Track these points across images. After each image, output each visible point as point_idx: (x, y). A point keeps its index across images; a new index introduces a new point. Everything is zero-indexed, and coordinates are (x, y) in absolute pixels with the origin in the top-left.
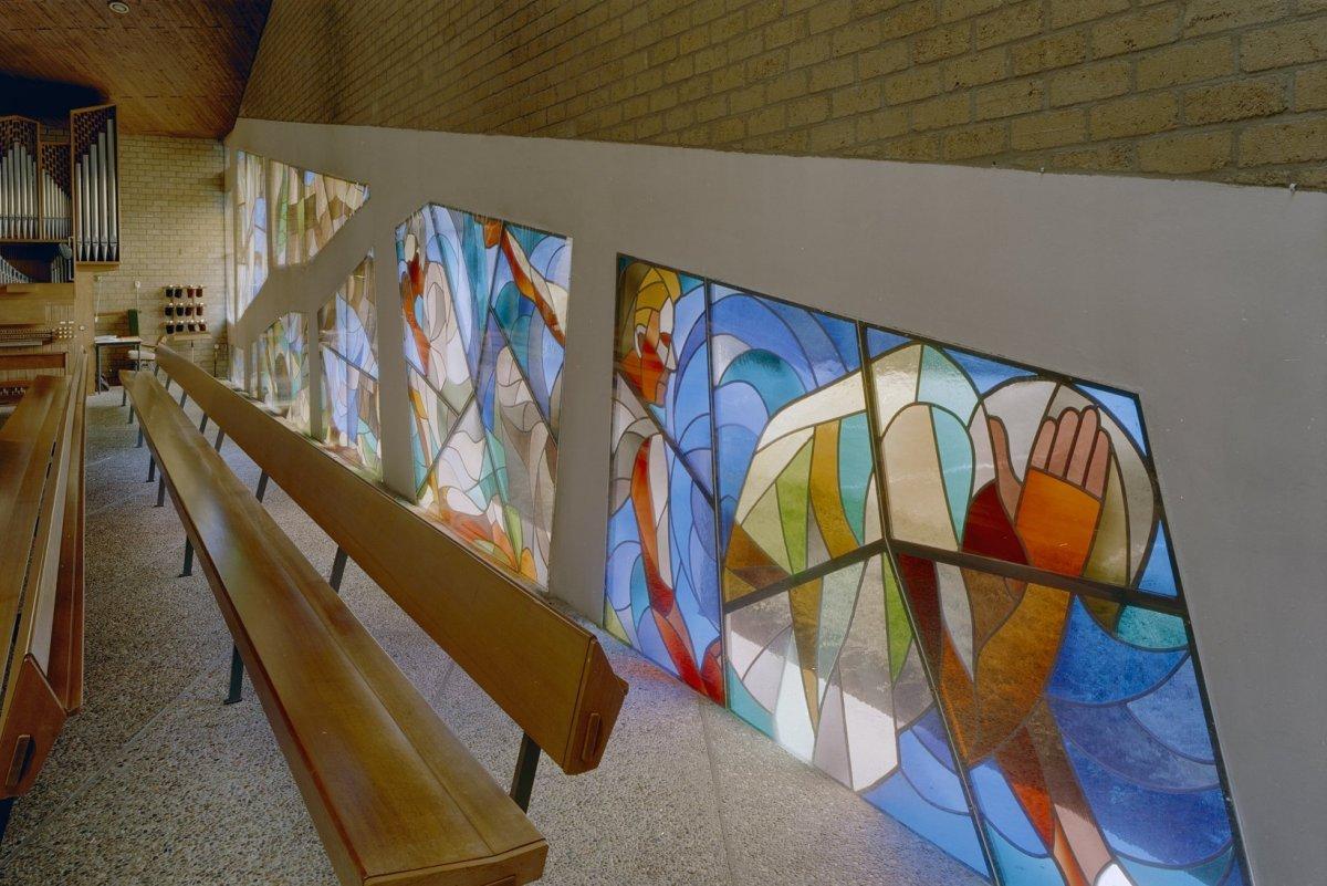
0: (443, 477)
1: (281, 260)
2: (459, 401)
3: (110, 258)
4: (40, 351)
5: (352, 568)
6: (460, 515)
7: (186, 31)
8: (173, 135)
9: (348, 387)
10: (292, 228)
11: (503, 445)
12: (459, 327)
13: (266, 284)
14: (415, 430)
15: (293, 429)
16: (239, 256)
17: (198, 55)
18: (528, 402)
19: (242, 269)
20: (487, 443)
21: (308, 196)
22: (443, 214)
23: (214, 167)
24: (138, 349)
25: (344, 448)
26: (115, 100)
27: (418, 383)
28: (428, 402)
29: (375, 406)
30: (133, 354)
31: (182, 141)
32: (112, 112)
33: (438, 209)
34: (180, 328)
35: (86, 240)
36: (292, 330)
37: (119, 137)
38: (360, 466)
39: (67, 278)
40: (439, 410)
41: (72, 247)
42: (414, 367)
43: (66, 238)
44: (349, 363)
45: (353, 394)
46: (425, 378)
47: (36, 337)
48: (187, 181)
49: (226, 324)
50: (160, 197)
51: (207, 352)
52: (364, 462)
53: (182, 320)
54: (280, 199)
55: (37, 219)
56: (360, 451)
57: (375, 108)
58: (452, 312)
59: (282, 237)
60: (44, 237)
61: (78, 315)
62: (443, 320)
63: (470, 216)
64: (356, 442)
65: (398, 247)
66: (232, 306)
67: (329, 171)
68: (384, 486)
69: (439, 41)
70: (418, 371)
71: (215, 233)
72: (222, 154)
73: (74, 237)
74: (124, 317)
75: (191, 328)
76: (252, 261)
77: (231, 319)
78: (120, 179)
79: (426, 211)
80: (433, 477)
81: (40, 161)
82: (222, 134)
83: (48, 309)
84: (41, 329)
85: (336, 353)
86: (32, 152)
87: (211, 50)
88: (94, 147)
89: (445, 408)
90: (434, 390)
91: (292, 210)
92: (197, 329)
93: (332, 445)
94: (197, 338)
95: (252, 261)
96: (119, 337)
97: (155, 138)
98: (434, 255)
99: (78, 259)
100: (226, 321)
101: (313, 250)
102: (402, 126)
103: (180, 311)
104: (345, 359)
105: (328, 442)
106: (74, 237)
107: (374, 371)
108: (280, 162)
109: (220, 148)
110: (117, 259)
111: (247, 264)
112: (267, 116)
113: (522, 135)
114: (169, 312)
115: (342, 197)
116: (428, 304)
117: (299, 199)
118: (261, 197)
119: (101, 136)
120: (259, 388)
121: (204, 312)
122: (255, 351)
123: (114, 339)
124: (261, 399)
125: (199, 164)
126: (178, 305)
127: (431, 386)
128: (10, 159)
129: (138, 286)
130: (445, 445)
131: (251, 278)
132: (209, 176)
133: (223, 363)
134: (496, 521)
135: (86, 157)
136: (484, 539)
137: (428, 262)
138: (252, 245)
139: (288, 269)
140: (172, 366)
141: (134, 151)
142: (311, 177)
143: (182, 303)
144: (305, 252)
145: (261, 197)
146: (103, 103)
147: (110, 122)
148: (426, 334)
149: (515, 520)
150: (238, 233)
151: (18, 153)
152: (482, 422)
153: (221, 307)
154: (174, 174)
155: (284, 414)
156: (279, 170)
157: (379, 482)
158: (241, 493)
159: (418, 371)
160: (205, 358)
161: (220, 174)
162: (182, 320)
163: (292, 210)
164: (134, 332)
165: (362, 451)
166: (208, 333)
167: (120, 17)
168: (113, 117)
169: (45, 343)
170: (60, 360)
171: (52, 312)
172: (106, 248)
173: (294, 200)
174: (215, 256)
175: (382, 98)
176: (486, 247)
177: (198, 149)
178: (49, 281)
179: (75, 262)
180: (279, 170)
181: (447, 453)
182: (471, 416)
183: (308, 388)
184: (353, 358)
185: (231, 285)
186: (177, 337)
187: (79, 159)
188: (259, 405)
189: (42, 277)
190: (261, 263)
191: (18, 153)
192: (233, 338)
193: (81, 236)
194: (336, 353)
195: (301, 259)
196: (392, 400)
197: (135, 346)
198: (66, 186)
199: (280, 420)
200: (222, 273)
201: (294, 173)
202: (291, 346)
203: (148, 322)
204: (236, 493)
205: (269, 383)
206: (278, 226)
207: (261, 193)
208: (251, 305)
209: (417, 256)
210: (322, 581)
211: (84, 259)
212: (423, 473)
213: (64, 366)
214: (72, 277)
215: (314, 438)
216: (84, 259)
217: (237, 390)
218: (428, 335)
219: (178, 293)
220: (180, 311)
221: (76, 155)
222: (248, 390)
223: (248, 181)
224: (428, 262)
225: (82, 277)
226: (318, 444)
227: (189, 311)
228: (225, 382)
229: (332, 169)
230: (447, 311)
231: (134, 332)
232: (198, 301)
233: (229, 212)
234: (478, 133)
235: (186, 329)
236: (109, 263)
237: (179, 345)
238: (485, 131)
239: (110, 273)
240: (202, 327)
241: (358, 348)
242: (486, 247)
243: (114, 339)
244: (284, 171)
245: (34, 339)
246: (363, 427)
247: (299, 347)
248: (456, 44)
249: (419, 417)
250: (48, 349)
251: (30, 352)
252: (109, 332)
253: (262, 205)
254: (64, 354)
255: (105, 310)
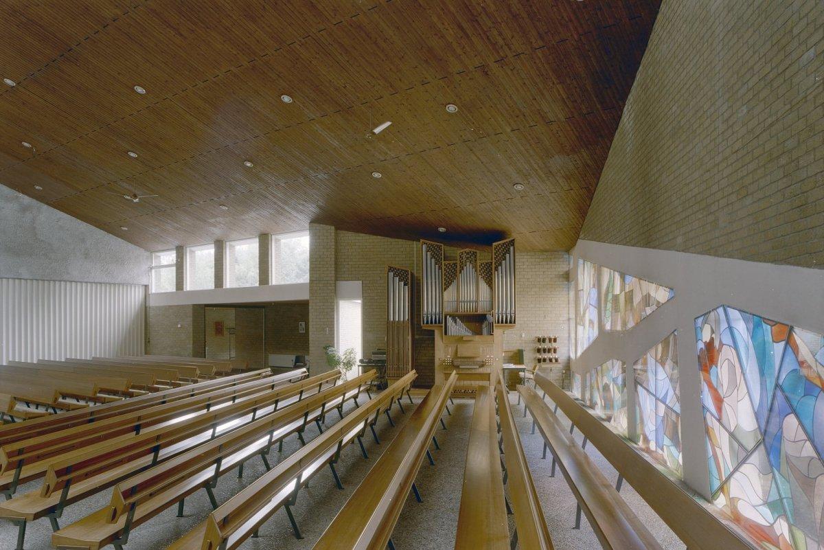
0: (734, 488)
1: (608, 327)
2: (750, 445)
4: (477, 371)
6: (747, 520)
7: (553, 194)
8: (542, 251)
9: (656, 414)
10: (616, 309)
11: (789, 482)
12: (748, 392)
13: (595, 342)
14: (710, 453)
15: (615, 432)
16: (579, 319)
17: (559, 207)
18: (813, 458)
19: (580, 328)
20: (774, 477)
21: (627, 290)
22: (734, 314)
23: (563, 268)
24: (524, 372)
25: (652, 451)
26: (514, 235)
27: (712, 422)
28: (722, 438)
29: (677, 432)
30: (522, 374)
32: (512, 242)
33: (730, 311)
34: (545, 360)
36: (613, 372)
37: (516, 254)
38: (664, 464)
39: (491, 333)
40: (730, 443)
42: (708, 410)
43: (490, 311)
44: (657, 399)
45: (659, 420)
46: (719, 420)
47: (475, 363)
49: (569, 359)
52: (668, 464)
53: (546, 356)
54: (608, 288)
55: (476, 302)
56: (666, 458)
57: (680, 240)
58: (743, 382)
59: (608, 313)
60: (480, 312)
61: (494, 352)
62: (734, 384)
63: (757, 320)
64: (662, 449)
65: (697, 331)
66: (574, 348)
67: (643, 276)
68: (684, 483)
69: (733, 198)
70: (712, 415)
74: (516, 353)
75: (551, 360)
76: (587, 323)
77: (573, 356)
79: (721, 310)
80: (725, 487)
81: (478, 271)
82: (568, 250)
83: (481, 349)
84: (478, 359)
85: (648, 390)
86: (475, 267)
87: (566, 203)
89: (736, 445)
90: (726, 430)
91: (616, 298)
92: (554, 361)
93: (643, 447)
94: (554, 366)
95: (587, 323)
96: (515, 364)
97: (533, 253)
98: (727, 339)
100: (569, 357)
101: (631, 324)
102: (701, 253)
103: (544, 351)
104: (655, 396)
105: (641, 444)
107: (677, 408)
108: (607, 267)
109: (567, 256)
110: (514, 323)
111: (584, 325)
112: (600, 239)
113: (808, 267)
114: (539, 351)
115: (653, 294)
116: (721, 372)
117: (621, 291)
118: (594, 287)
119: (507, 255)
120: (591, 400)
122: (588, 378)
123: (512, 366)
124: (592, 407)
125: (555, 266)
126: (544, 347)
127: (724, 427)
128: (465, 271)
129: (523, 336)
130: (736, 470)
131: (586, 335)
134: (782, 534)
136: (769, 542)
137: (721, 344)
138: (587, 315)
139: (612, 333)
140: (541, 382)
141: (523, 262)
142: (629, 279)
143: (546, 345)
144: (624, 324)
145: (594, 287)
146: (506, 239)
147: (512, 248)
148: (720, 391)
149: (800, 535)
150: (578, 309)
151: (469, 267)
152: (769, 461)
153: (567, 348)
155: (609, 419)
156: (606, 273)
157: (681, 480)
158: (608, 486)
159: (712, 415)
160: (558, 378)
162: (546, 356)
163: (616, 298)
164: (521, 361)
165: (669, 459)
167: (519, 192)
168: (513, 245)
169: (480, 367)
170: (487, 377)
171: (483, 350)
173: (617, 291)
175: (685, 233)
176: (773, 341)
178: (482, 334)
180: (606, 273)
181: (737, 475)
182: (756, 458)
183: (626, 408)
184: (661, 396)
185: (573, 335)
186: (544, 365)
187: (496, 269)
188: (591, 412)
189: (479, 332)
190: (593, 327)
191: (469, 267)
192: (573, 368)
194: (648, 390)
195: (622, 327)
196: (691, 427)
197: (523, 370)
198: (490, 283)
199: (606, 424)
200: (567, 328)
201: (617, 276)
202: (614, 380)
203: (529, 356)
204: (604, 485)
205: (598, 399)
206: (606, 307)
207: (594, 285)
208: (586, 350)
209: (712, 339)
211: (498, 322)
212: (716, 484)
213: (489, 380)
215: (630, 440)
216: (498, 322)
217: (577, 399)
218: (723, 391)
219: (544, 340)
220: (544, 351)
222: (583, 400)
223: (585, 276)
224: (721, 344)
225: (497, 332)
226: (635, 445)
227: (549, 351)
228: (568, 393)
229: (645, 275)
230: (738, 382)
231: (521, 361)
232: (554, 345)
233: (572, 294)
234: (768, 262)
235: (548, 361)
237: (544, 370)
238: (775, 261)
241: (664, 392)
242: (773, 341)
243: (512, 366)
244: (610, 273)
245: (475, 364)
246: (667, 441)
247: (620, 381)
248: (749, 200)
249: (713, 446)
250: (481, 370)
251: (473, 371)
252: (509, 362)
253: (594, 292)
254: (490, 374)
255: (507, 350)
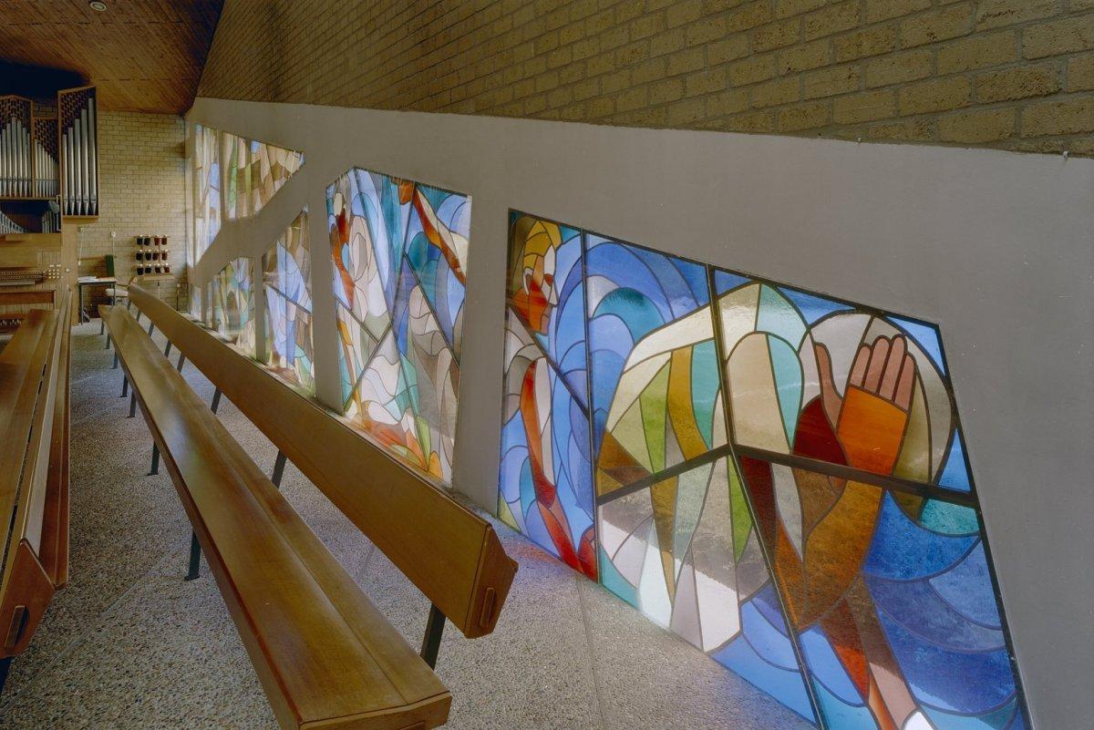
0: (365, 393)
1: (232, 214)
2: (379, 330)
3: (90, 213)
4: (33, 289)
5: (290, 468)
6: (379, 424)
7: (153, 25)
8: (143, 111)
9: (287, 319)
10: (241, 188)
11: (415, 367)
12: (378, 270)
13: (219, 234)
14: (342, 354)
15: (242, 354)
16: (197, 211)
17: (163, 46)
18: (435, 331)
19: (199, 222)
20: (401, 365)
21: (254, 161)
22: (365, 177)
23: (176, 138)
24: (114, 287)
25: (284, 369)
26: (95, 82)
27: (344, 315)
28: (353, 331)
29: (309, 335)
30: (110, 291)
31: (150, 116)
32: (92, 93)
33: (361, 172)
34: (148, 270)
35: (71, 198)
36: (241, 272)
37: (98, 113)
38: (297, 384)
39: (55, 229)
40: (362, 338)
41: (59, 204)
42: (341, 302)
43: (54, 196)
44: (287, 299)
45: (291, 324)
46: (351, 311)
47: (30, 277)
48: (154, 149)
49: (186, 267)
50: (132, 162)
51: (170, 290)
52: (300, 381)
53: (150, 264)
54: (231, 164)
55: (30, 180)
56: (297, 372)
57: (309, 89)
58: (373, 257)
59: (232, 195)
60: (36, 195)
61: (65, 259)
62: (365, 264)
63: (387, 178)
64: (294, 364)
65: (328, 204)
66: (192, 252)
67: (272, 141)
68: (316, 400)
69: (362, 34)
70: (344, 306)
71: (177, 192)
72: (183, 127)
73: (61, 195)
74: (102, 261)
75: (158, 270)
76: (208, 215)
77: (190, 263)
78: (99, 147)
79: (351, 174)
80: (357, 393)
81: (33, 133)
82: (183, 110)
83: (39, 255)
84: (34, 271)
85: (277, 291)
86: (27, 126)
87: (174, 41)
88: (77, 121)
89: (367, 336)
90: (358, 321)
91: (241, 173)
92: (163, 271)
93: (274, 367)
94: (162, 278)
95: (208, 215)
96: (98, 277)
97: (128, 114)
98: (358, 210)
99: (64, 214)
100: (186, 264)
101: (258, 206)
102: (331, 104)
103: (148, 256)
104: (285, 296)
105: (271, 364)
106: (61, 195)
107: (308, 306)
108: (231, 133)
109: (182, 122)
110: (97, 214)
111: (203, 217)
112: (220, 96)
113: (430, 112)
114: (139, 257)
115: (282, 163)
116: (353, 250)
117: (247, 164)
118: (215, 162)
119: (84, 112)
120: (213, 319)
121: (168, 257)
122: (210, 289)
123: (94, 279)
124: (215, 329)
125: (164, 135)
126: (147, 252)
127: (355, 318)
128: (9, 131)
129: (114, 236)
130: (367, 367)
131: (207, 229)
132: (172, 145)
133: (184, 299)
134: (409, 429)
135: (71, 129)
136: (399, 444)
137: (353, 216)
138: (207, 202)
139: (237, 222)
140: (142, 302)
141: (110, 125)
142: (256, 146)
143: (150, 249)
144: (251, 207)
145: (215, 162)
146: (85, 85)
147: (90, 100)
148: (351, 275)
149: (425, 428)
150: (197, 192)
151: (15, 126)
152: (397, 347)
153: (182, 253)
154: (143, 144)
155: (234, 341)
156: (230, 140)
157: (313, 397)
159: (344, 306)
160: (169, 295)
161: (182, 143)
162: (150, 264)
163: (241, 173)
164: (111, 274)
165: (299, 372)
166: (171, 274)
167: (99, 14)
168: (94, 97)
169: (37, 282)
170: (49, 297)
171: (43, 257)
172: (88, 204)
173: (243, 165)
174: (177, 211)
175: (315, 81)
176: (401, 204)
177: (163, 123)
178: (41, 231)
179: (62, 216)
180: (230, 140)
181: (369, 373)
182: (389, 343)
183: (254, 320)
184: (291, 295)
185: (190, 234)
186: (146, 278)
187: (65, 131)
188: (214, 334)
189: (34, 228)
190: (215, 217)
191: (15, 126)
192: (192, 279)
193: (66, 195)
194: (277, 291)
195: (249, 213)
196: (323, 330)
197: (111, 285)
198: (54, 153)
199: (231, 346)
200: (183, 225)
201: (242, 142)
202: (240, 285)
203: (122, 265)
204: (195, 406)
205: (222, 316)
206: (229, 186)
207: (215, 159)
208: (207, 251)
209: (343, 211)
210: (266, 479)
211: (69, 213)
212: (349, 390)
213: (53, 302)
214: (60, 228)
215: (259, 361)
216: (69, 213)
217: (196, 321)
218: (353, 276)
219: (147, 241)
220: (148, 256)
221: (62, 128)
222: (204, 321)
223: (204, 149)
224: (353, 216)
225: (67, 229)
226: (263, 366)
227: (155, 256)
228: (185, 315)
229: (274, 139)
230: (369, 256)
231: (111, 274)
232: (163, 248)
233: (189, 175)
234: (394, 109)
235: (153, 271)
236: (90, 217)
237: (148, 285)
238: (400, 108)
239: (90, 225)
240: (167, 270)
241: (296, 287)
242: (401, 204)
243: (94, 279)
244: (234, 141)
245: (28, 279)
246: (299, 352)
247: (247, 286)
248: (376, 36)
249: (345, 344)
250: (40, 288)
251: (25, 290)
252: (90, 274)
253: (216, 169)
254: (53, 292)
255: (86, 256)
